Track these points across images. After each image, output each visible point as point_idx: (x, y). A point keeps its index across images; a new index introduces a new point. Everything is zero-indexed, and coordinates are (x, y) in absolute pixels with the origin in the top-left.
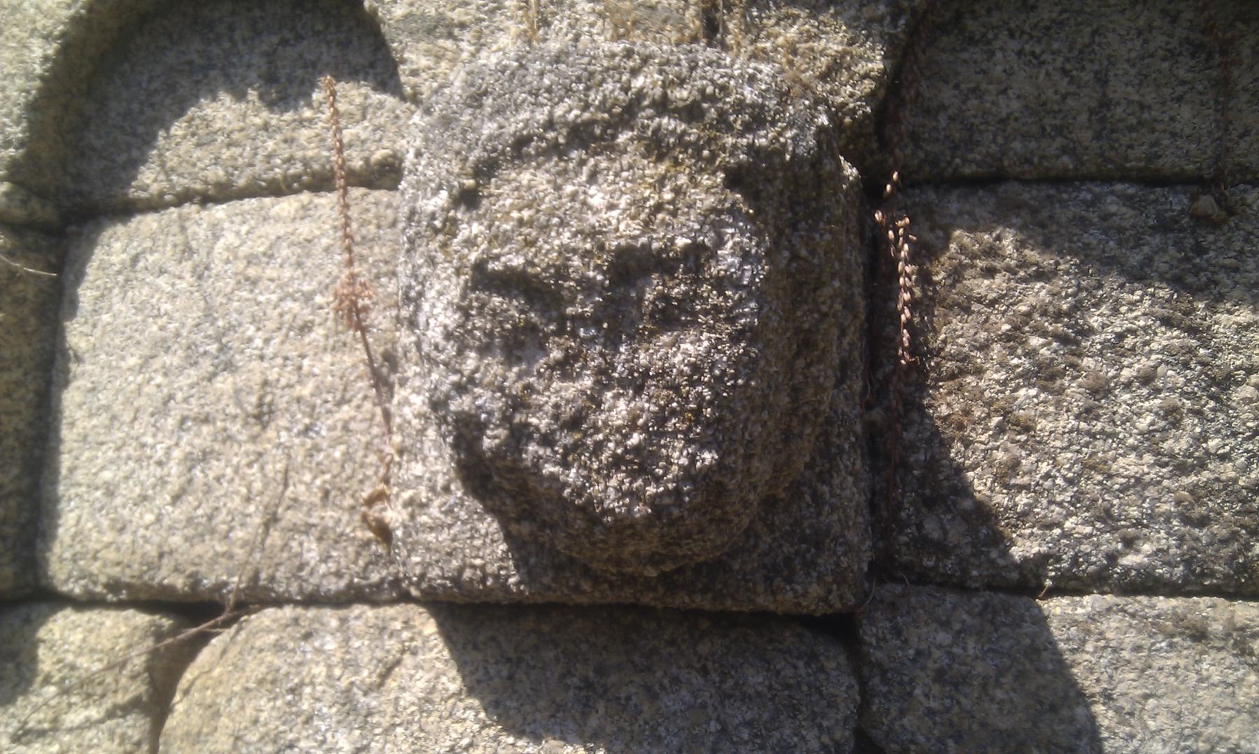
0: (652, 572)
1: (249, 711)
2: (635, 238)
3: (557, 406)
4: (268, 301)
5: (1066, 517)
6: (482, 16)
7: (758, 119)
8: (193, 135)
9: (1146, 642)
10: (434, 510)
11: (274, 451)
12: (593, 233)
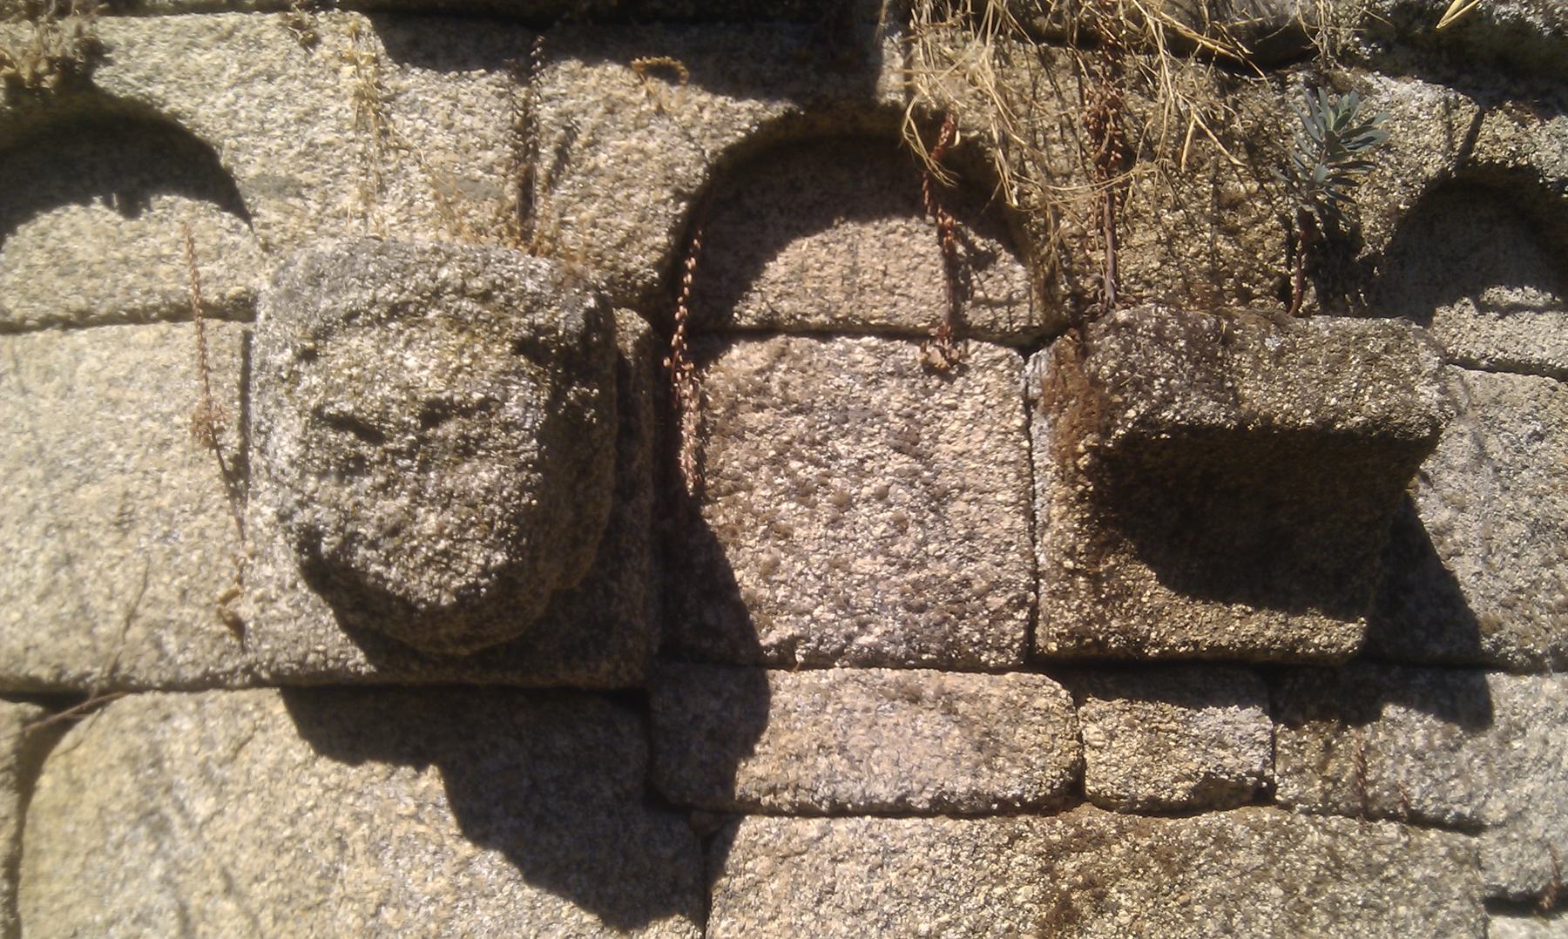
0: (464, 651)
1: (113, 784)
2: (441, 392)
3: (381, 519)
4: (129, 420)
5: (816, 607)
6: (328, 179)
7: (537, 303)
8: (55, 265)
9: (873, 705)
10: (283, 605)
11: (135, 556)
12: (407, 388)
